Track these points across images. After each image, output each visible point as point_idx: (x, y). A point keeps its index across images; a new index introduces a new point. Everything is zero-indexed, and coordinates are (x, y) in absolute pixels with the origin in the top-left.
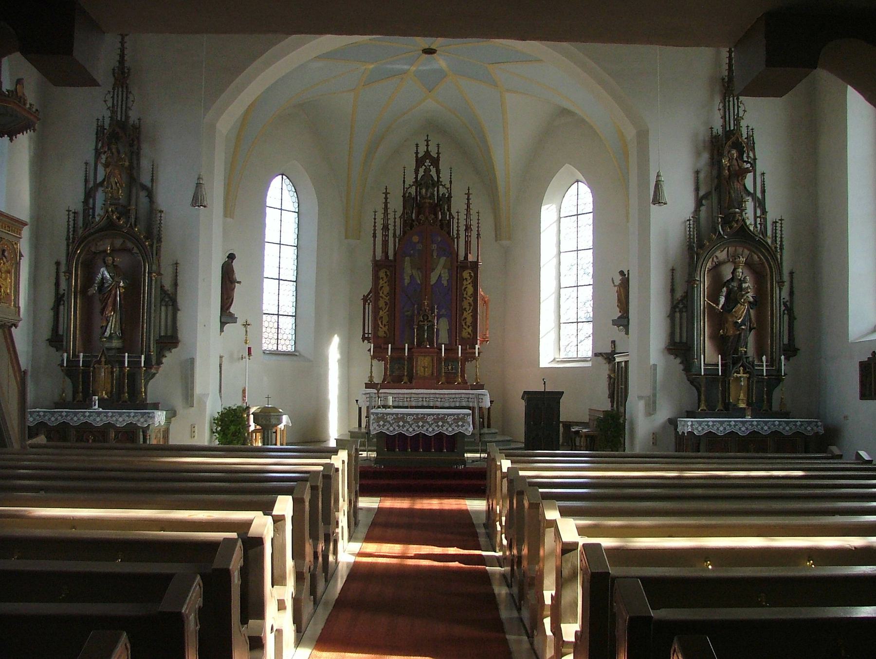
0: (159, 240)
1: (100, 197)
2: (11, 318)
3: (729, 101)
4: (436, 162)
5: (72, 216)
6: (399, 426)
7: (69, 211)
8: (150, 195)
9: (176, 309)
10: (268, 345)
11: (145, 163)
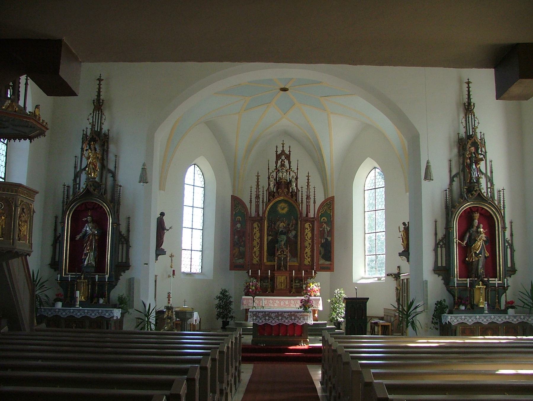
0: (119, 204)
1: (83, 177)
2: (26, 249)
3: (469, 117)
4: (288, 157)
5: (66, 188)
6: (265, 319)
7: (64, 185)
8: (114, 176)
9: (128, 247)
10: (185, 268)
11: (111, 156)
